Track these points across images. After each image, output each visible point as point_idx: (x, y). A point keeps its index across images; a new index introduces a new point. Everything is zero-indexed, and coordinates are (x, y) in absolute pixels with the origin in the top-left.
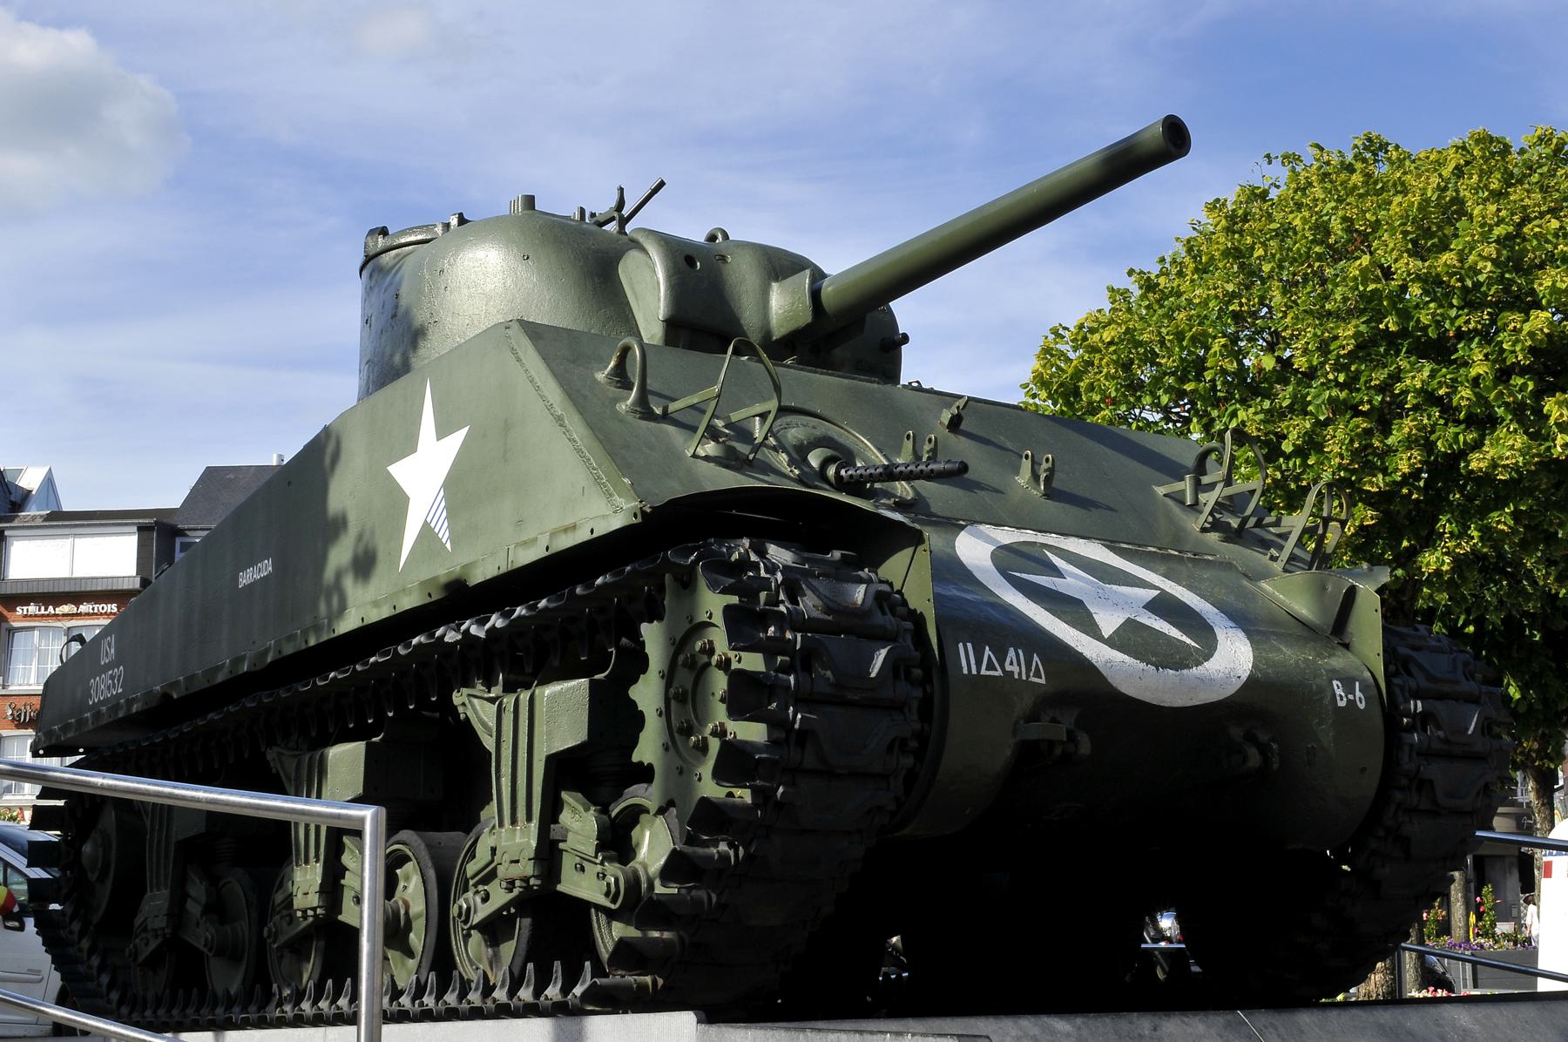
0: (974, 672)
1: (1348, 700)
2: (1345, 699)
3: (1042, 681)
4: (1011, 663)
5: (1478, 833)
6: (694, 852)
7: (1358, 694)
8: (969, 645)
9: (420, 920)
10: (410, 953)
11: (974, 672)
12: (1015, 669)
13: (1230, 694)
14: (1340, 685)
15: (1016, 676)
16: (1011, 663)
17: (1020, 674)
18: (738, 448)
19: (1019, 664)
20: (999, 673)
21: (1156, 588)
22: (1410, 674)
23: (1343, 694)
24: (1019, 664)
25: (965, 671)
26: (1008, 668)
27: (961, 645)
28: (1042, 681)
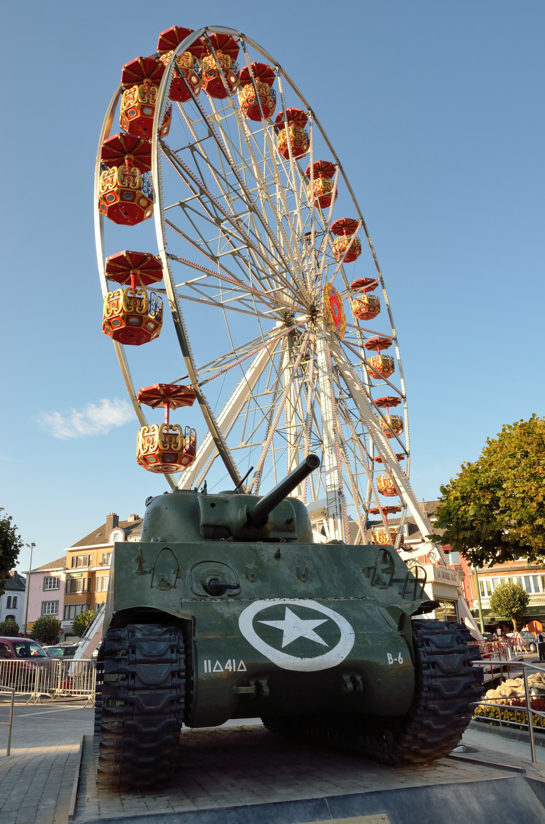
0: (210, 671)
1: (394, 661)
2: (393, 661)
3: (245, 670)
4: (228, 666)
5: (256, 722)
6: (220, 729)
7: (400, 658)
8: (209, 661)
9: (410, 594)
10: (426, 536)
11: (210, 671)
12: (230, 668)
13: (339, 663)
14: (391, 655)
15: (230, 670)
16: (228, 666)
17: (232, 669)
18: (154, 205)
19: (232, 665)
20: (222, 670)
21: (323, 616)
22: (428, 645)
23: (392, 659)
24: (232, 665)
25: (206, 671)
26: (226, 667)
27: (205, 661)
28: (245, 670)
